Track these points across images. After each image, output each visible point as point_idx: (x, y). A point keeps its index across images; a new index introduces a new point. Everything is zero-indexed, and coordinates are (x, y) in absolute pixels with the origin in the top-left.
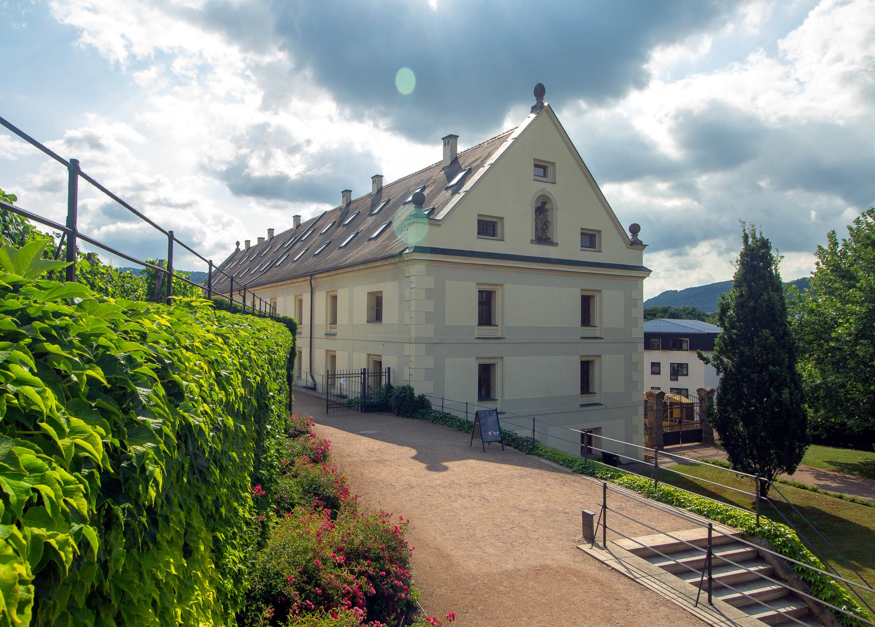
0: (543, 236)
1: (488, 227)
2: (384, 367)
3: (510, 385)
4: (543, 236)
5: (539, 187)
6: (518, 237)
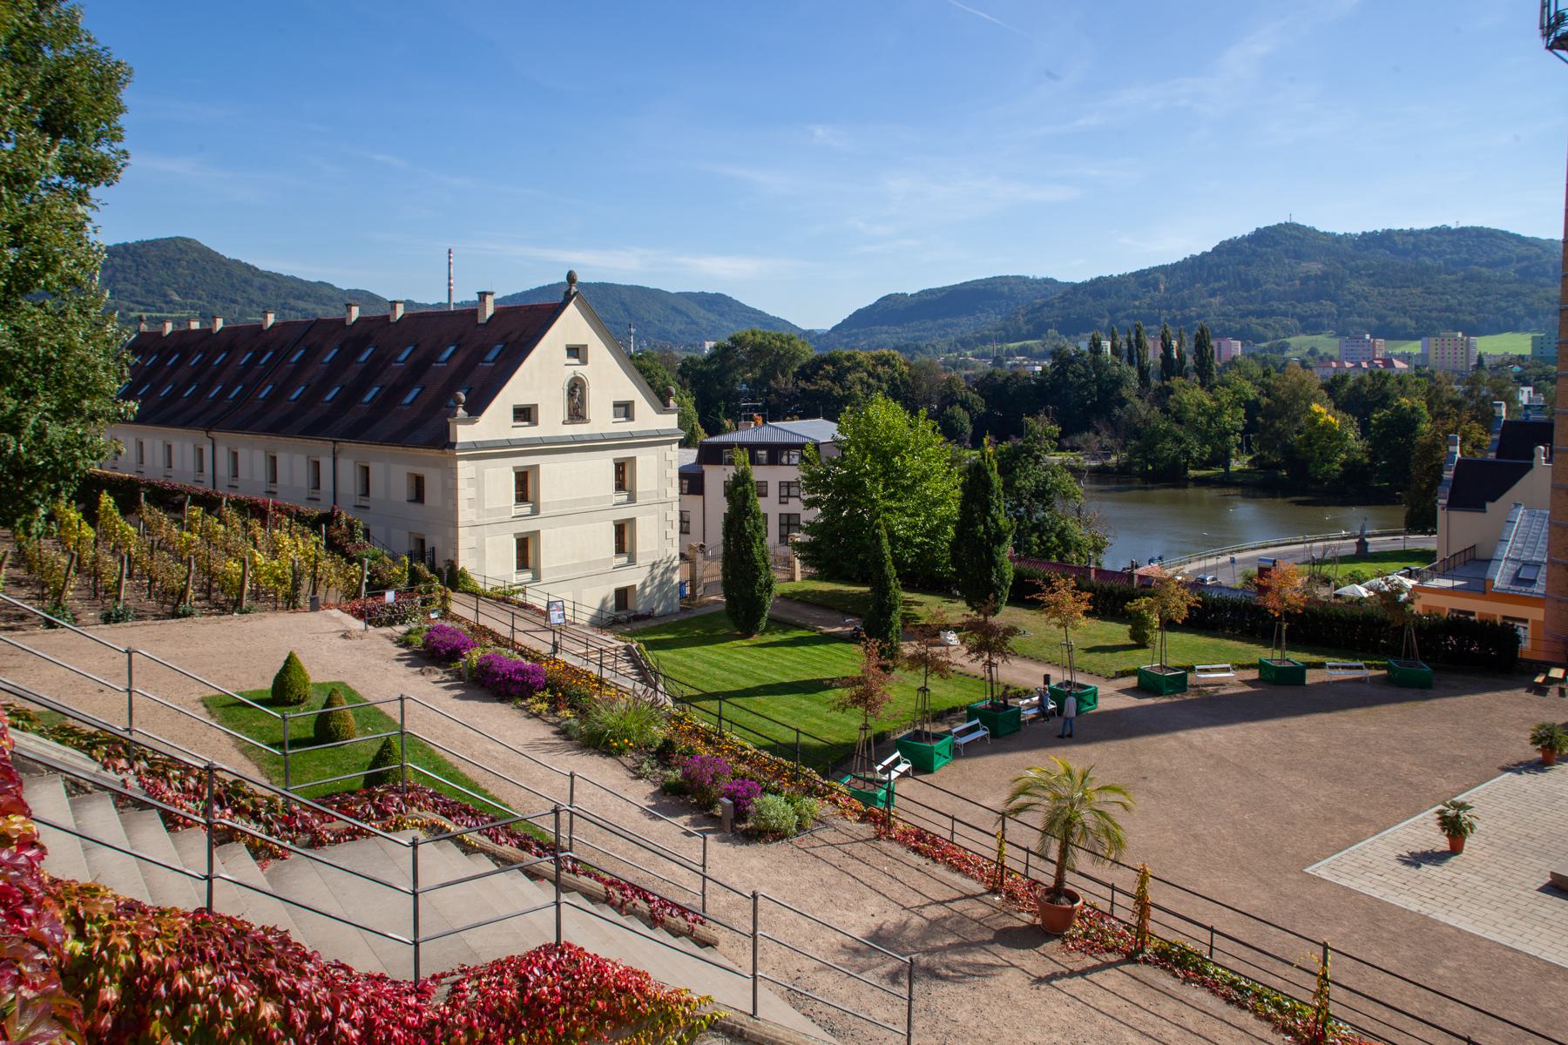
0: (577, 412)
1: (525, 414)
2: (428, 548)
3: (549, 555)
4: (577, 412)
5: (568, 373)
6: (552, 422)
